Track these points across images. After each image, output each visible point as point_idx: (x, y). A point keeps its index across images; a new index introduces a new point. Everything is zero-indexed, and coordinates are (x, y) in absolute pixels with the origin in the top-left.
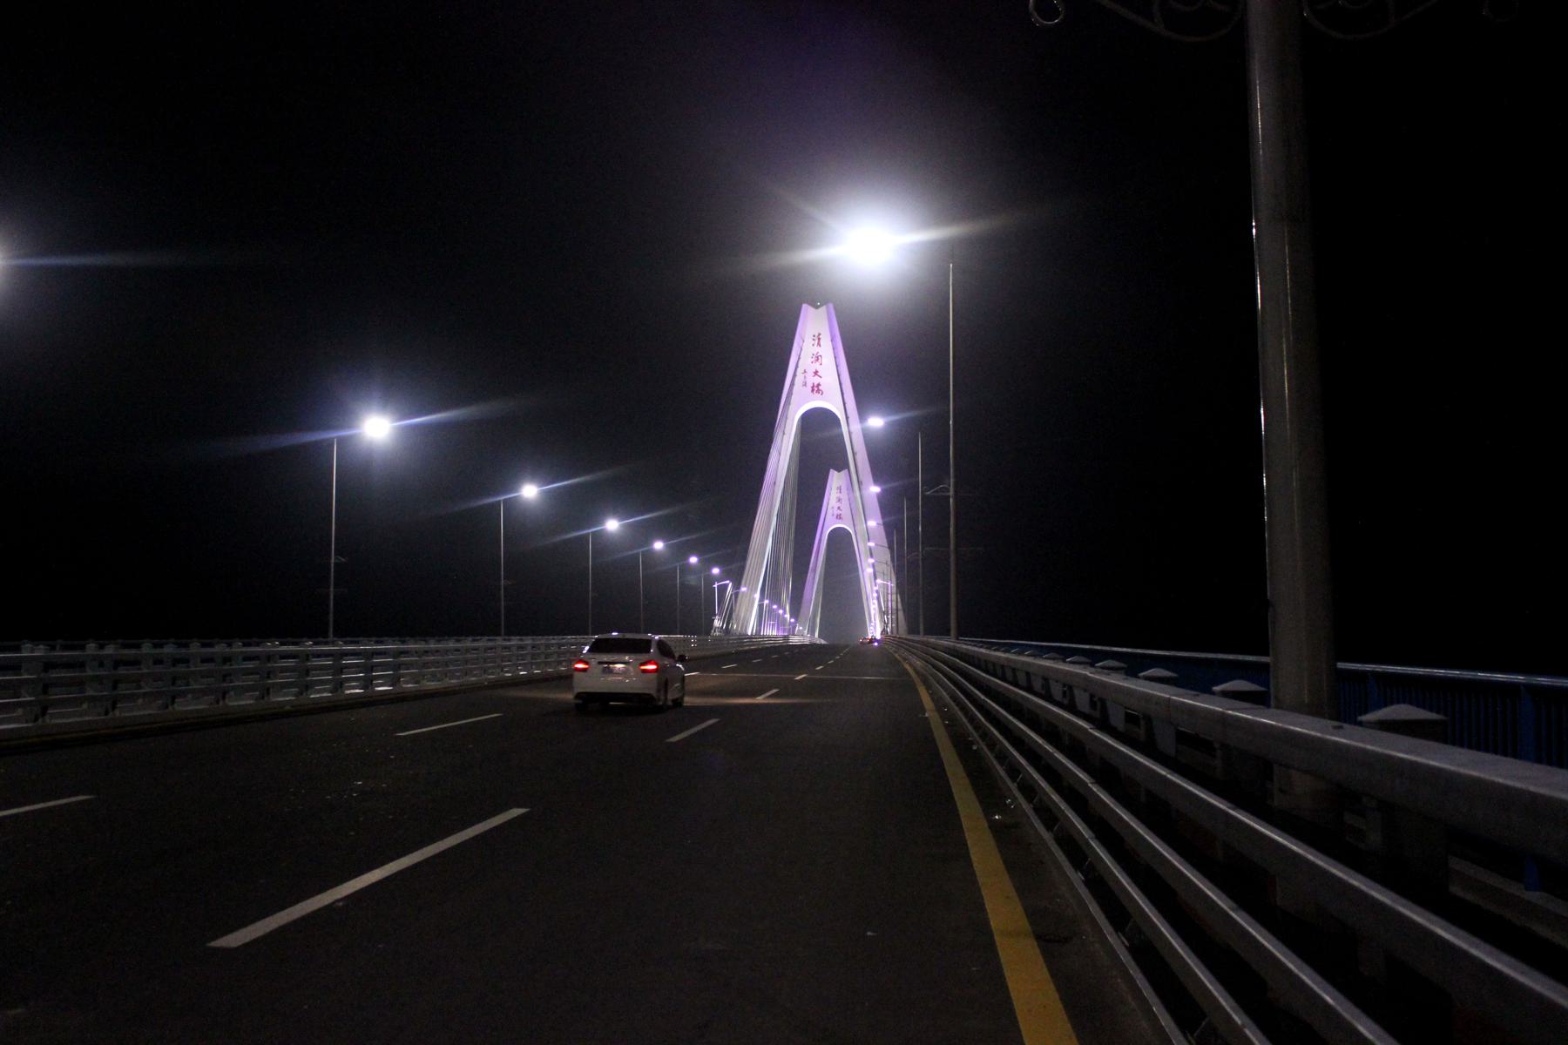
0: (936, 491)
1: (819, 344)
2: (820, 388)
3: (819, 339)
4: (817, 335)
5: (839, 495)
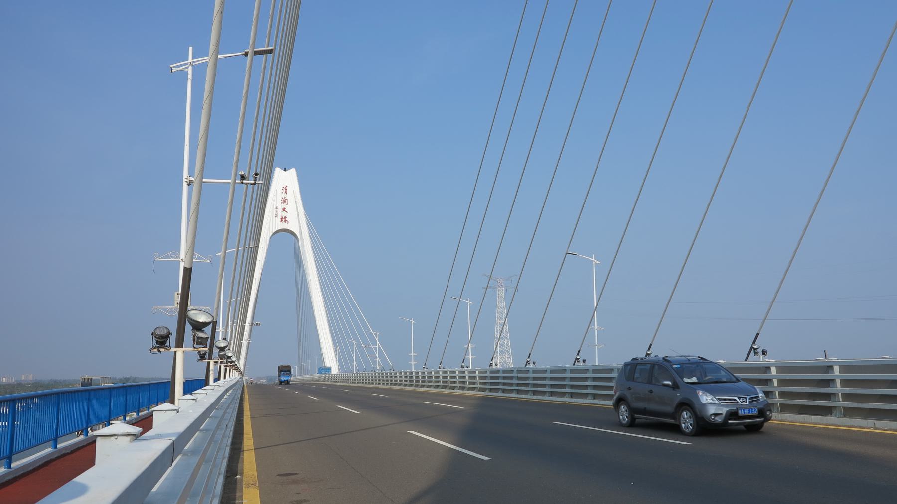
0: (205, 260)
1: (286, 193)
2: (286, 219)
3: (286, 189)
4: (285, 186)
5: (284, 195)
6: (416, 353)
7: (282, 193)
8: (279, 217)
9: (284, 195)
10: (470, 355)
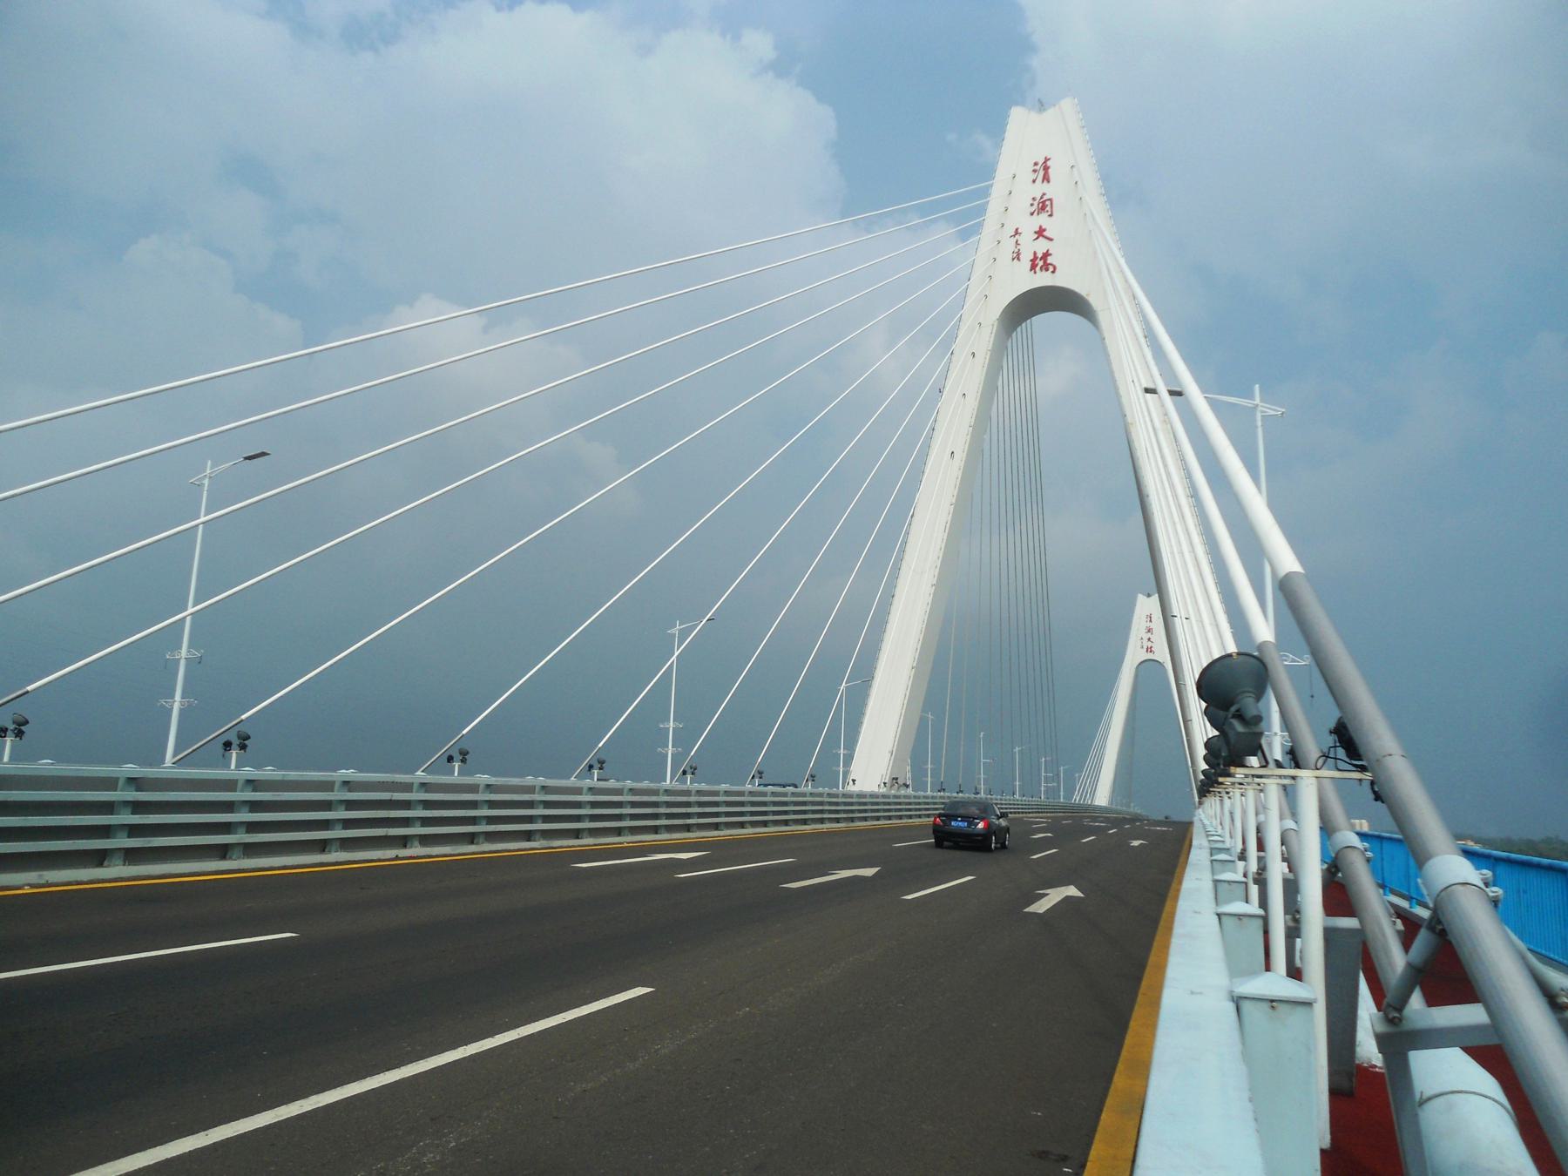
1: (1151, 621)
2: (1050, 260)
3: (1046, 169)
4: (1041, 161)
6: (848, 749)
7: (1034, 181)
8: (1145, 647)
9: (1039, 189)
10: (671, 729)
